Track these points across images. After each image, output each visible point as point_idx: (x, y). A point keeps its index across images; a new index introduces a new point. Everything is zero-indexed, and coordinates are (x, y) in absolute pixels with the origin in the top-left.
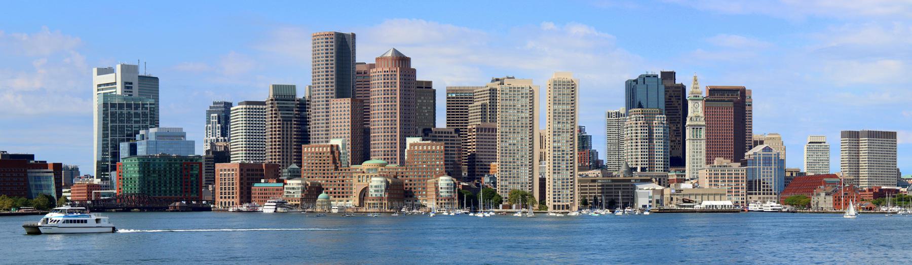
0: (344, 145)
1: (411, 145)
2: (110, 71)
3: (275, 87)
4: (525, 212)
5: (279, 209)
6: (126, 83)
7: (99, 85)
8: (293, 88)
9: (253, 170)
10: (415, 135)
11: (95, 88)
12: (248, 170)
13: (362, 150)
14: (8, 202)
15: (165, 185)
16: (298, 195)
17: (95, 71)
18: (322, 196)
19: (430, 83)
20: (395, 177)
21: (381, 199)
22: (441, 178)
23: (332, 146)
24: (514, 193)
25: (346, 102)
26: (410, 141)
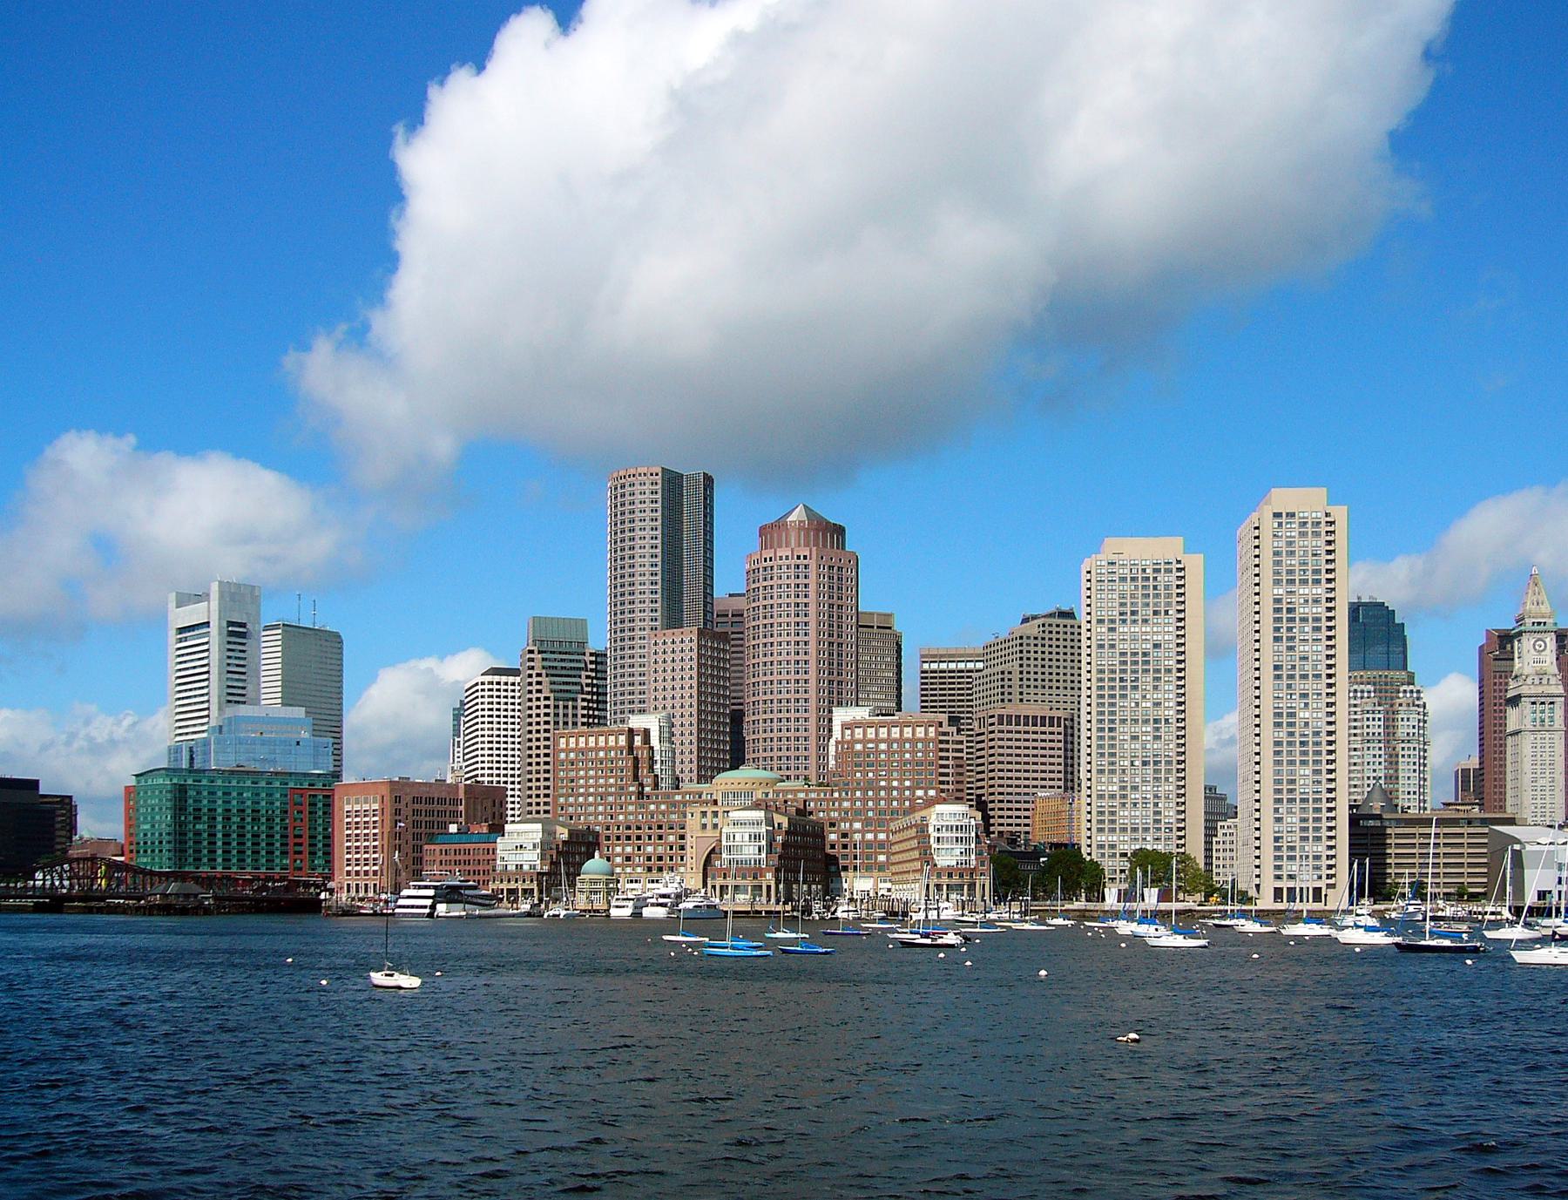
0: (668, 734)
1: (846, 726)
2: (201, 597)
4: (1083, 915)
5: (442, 908)
6: (230, 624)
7: (181, 630)
9: (430, 800)
10: (621, 921)
11: (172, 636)
12: (416, 800)
16: (531, 859)
17: (172, 597)
18: (595, 865)
20: (803, 812)
21: (757, 873)
22: (939, 808)
24: (1141, 858)
25: (686, 640)
26: (841, 715)
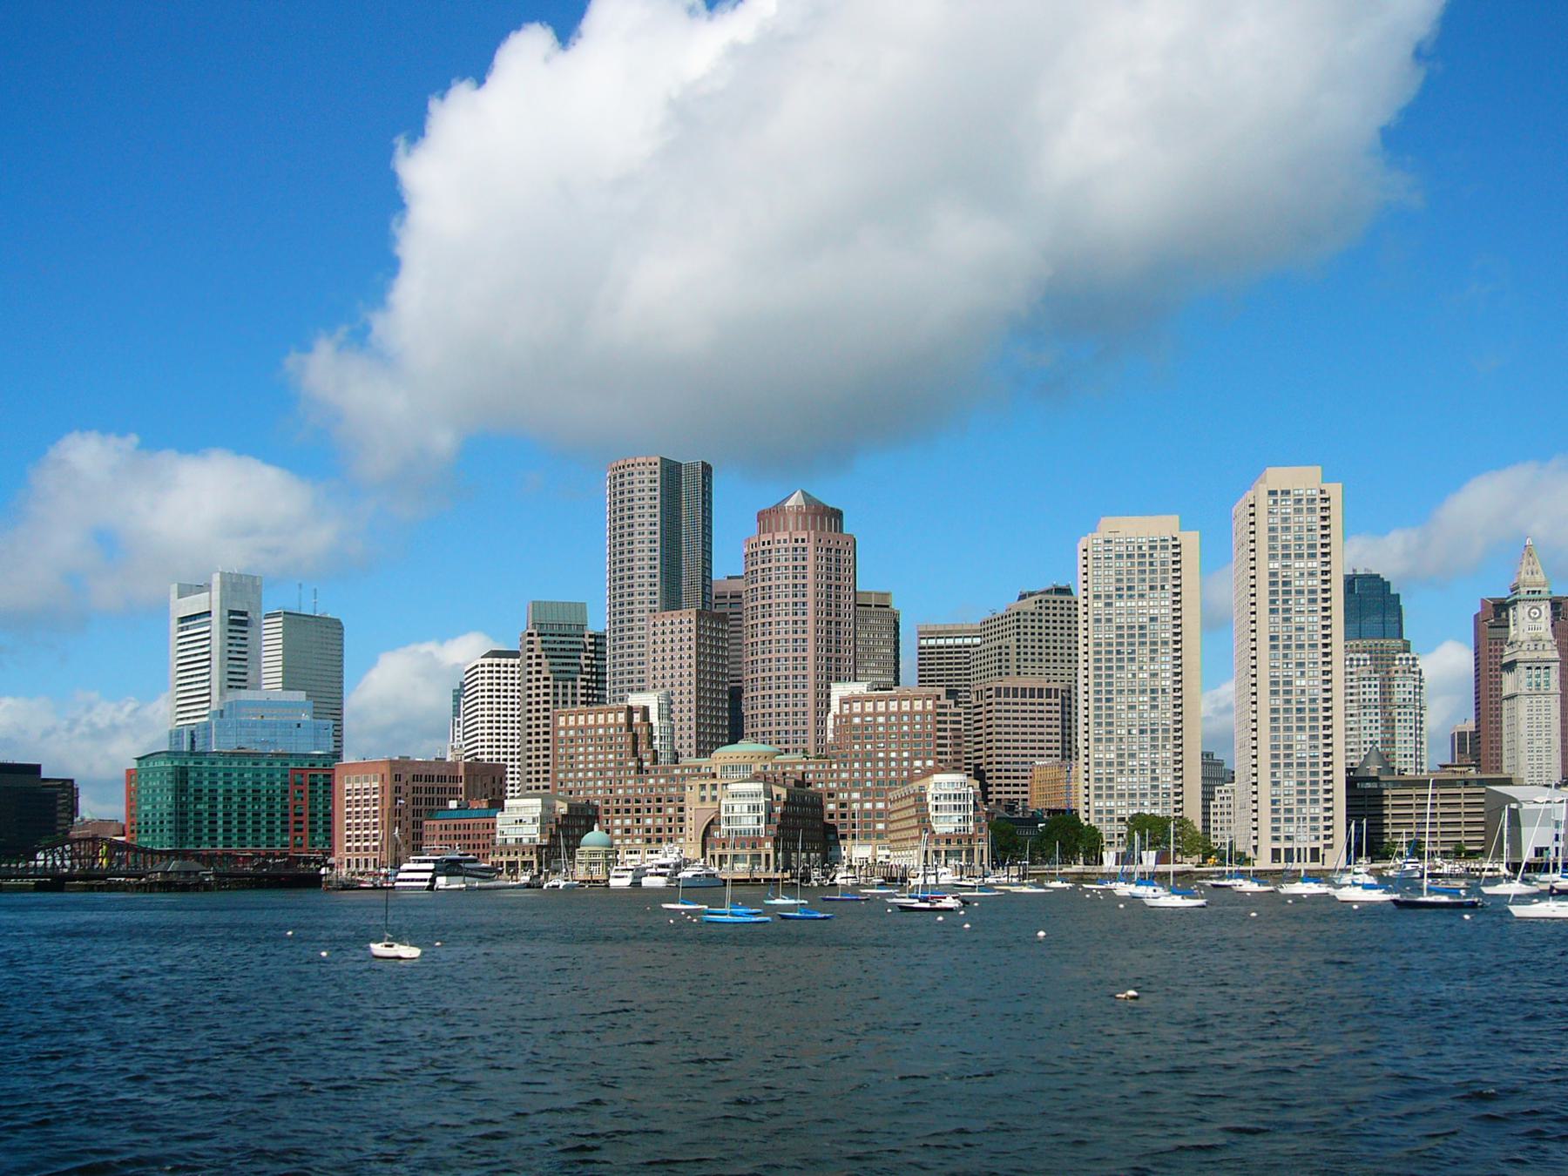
0: (667, 711)
1: (843, 701)
3: (536, 606)
5: (441, 881)
6: (232, 612)
7: (183, 619)
8: (582, 607)
9: (430, 778)
12: (416, 778)
13: (724, 716)
14: (1220, 715)
15: (256, 814)
16: (531, 832)
18: (595, 837)
19: (72, 781)
21: (755, 842)
22: (937, 778)
23: (630, 710)
24: (1139, 823)
26: (839, 691)
